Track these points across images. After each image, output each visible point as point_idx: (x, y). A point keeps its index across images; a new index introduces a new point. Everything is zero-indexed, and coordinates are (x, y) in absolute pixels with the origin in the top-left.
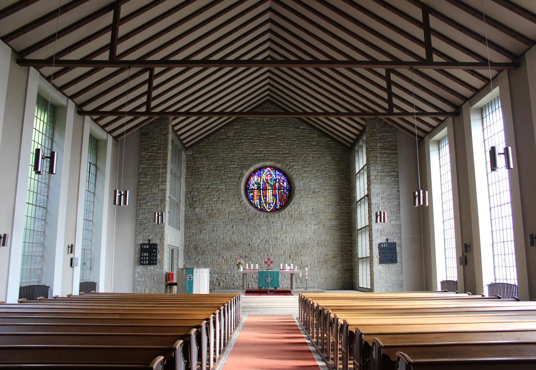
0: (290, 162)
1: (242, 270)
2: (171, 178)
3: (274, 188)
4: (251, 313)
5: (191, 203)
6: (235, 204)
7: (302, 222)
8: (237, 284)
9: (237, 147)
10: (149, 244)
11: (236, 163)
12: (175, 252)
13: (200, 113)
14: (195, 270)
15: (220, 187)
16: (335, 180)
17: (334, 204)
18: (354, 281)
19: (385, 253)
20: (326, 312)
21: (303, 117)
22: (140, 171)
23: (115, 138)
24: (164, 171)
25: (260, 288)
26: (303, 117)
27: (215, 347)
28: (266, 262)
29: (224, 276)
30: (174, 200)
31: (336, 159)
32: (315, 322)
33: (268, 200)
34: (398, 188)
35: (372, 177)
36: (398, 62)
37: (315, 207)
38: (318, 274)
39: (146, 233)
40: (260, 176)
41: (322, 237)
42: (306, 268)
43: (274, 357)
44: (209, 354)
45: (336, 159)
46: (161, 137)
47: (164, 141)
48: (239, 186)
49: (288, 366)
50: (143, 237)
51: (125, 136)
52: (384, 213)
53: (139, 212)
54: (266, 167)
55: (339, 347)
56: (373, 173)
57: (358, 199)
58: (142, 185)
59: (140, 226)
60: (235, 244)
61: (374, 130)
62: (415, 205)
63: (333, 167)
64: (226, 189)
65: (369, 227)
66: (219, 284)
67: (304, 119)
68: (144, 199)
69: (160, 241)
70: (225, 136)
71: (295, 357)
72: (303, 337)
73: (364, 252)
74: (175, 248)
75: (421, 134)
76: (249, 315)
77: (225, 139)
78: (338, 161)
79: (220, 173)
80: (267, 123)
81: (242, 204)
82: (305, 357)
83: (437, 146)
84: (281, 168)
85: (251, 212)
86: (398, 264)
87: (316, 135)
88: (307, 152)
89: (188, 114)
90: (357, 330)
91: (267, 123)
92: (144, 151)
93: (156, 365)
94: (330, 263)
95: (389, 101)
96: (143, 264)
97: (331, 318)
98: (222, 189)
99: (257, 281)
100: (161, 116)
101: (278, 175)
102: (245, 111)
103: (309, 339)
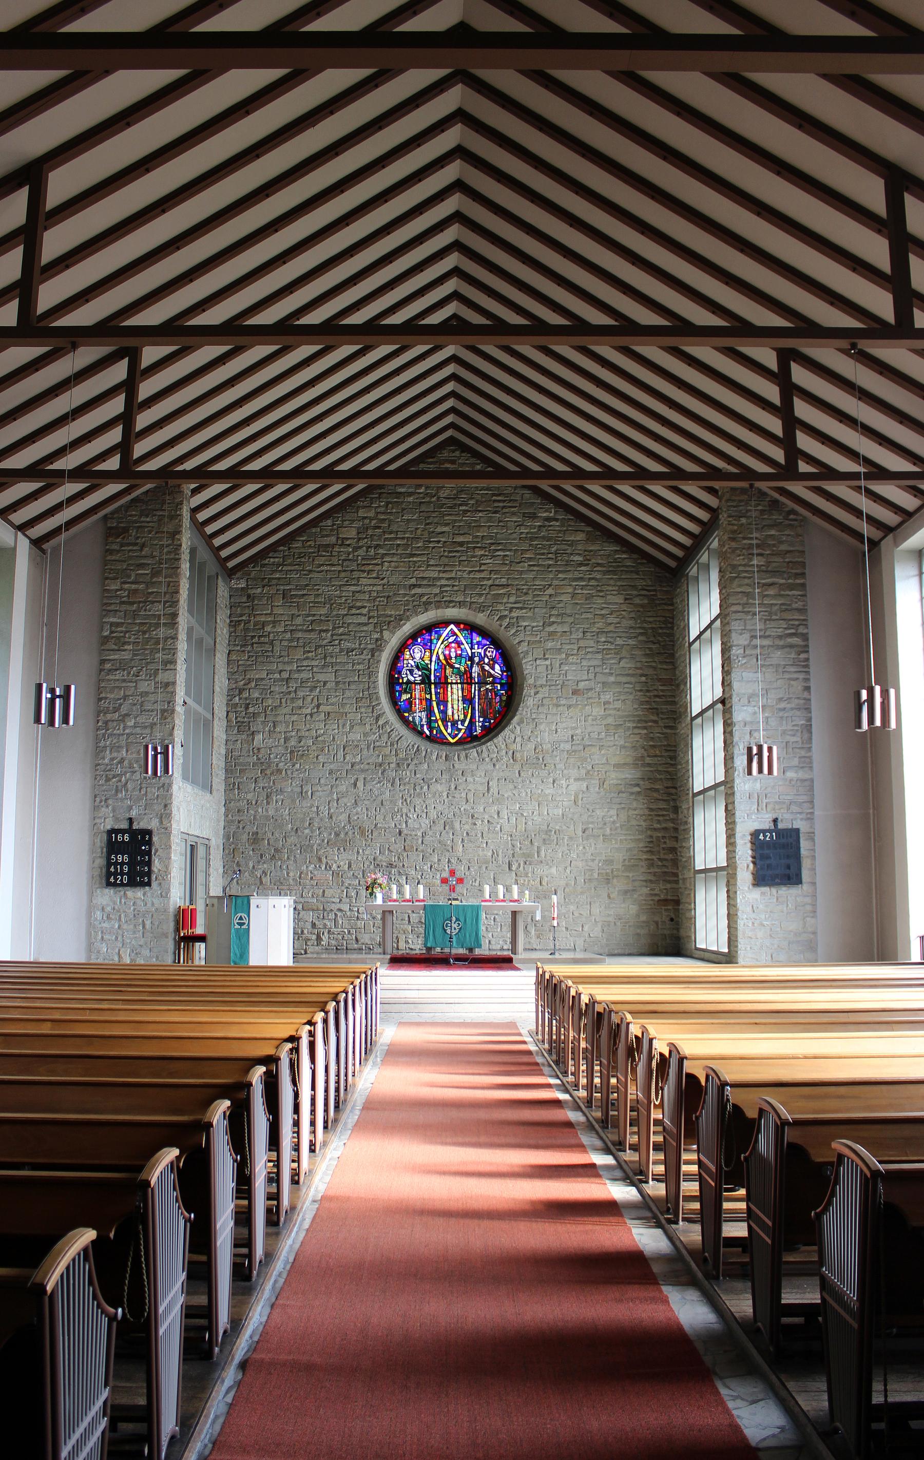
0: (511, 610)
1: (379, 900)
2: (188, 652)
3: (466, 679)
4: (407, 1018)
5: (243, 717)
6: (362, 723)
7: (544, 773)
8: (365, 938)
9: (367, 568)
10: (130, 831)
11: (365, 611)
12: (201, 852)
13: (269, 475)
14: (254, 902)
15: (321, 677)
16: (633, 657)
17: (630, 725)
18: (682, 933)
19: (768, 858)
20: (615, 1019)
21: (544, 485)
22: (106, 634)
23: (37, 543)
24: (170, 632)
25: (429, 949)
26: (544, 485)
27: (313, 1111)
28: (444, 881)
29: (332, 916)
30: (196, 713)
31: (637, 601)
32: (583, 1045)
33: (450, 712)
34: (807, 680)
35: (735, 651)
36: (810, 329)
37: (579, 731)
38: (585, 913)
39: (122, 800)
40: (428, 646)
41: (598, 812)
42: (554, 898)
43: (474, 1140)
44: (298, 1133)
45: (637, 601)
46: (161, 539)
47: (169, 553)
48: (371, 673)
49: (512, 1166)
50: (114, 811)
51: (63, 536)
52: (770, 749)
53: (102, 744)
54: (446, 624)
55: (656, 1115)
56: (739, 640)
57: (696, 710)
58: (110, 670)
59: (105, 780)
60: (362, 831)
61: (743, 520)
62: (860, 727)
63: (626, 623)
64: (337, 683)
65: (726, 787)
66: (319, 938)
67: (544, 487)
68: (116, 710)
69: (161, 822)
70: (333, 539)
71: (532, 1142)
72: (549, 1086)
73: (711, 855)
74: (200, 841)
75: (876, 534)
76: (401, 1024)
77: (333, 546)
78: (642, 606)
79: (321, 639)
80: (450, 503)
81: (381, 722)
82: (559, 1142)
83: (916, 565)
84: (487, 626)
85: (403, 744)
86: (805, 887)
87: (581, 536)
88: (555, 582)
89: (236, 475)
90: (712, 1074)
91: (450, 503)
92: (115, 578)
93: (157, 1173)
94: (620, 884)
95: (787, 442)
96: (114, 885)
97: (631, 1036)
98: (325, 683)
99: (422, 930)
100: (161, 482)
101: (478, 643)
102: (392, 467)
103: (567, 1091)
